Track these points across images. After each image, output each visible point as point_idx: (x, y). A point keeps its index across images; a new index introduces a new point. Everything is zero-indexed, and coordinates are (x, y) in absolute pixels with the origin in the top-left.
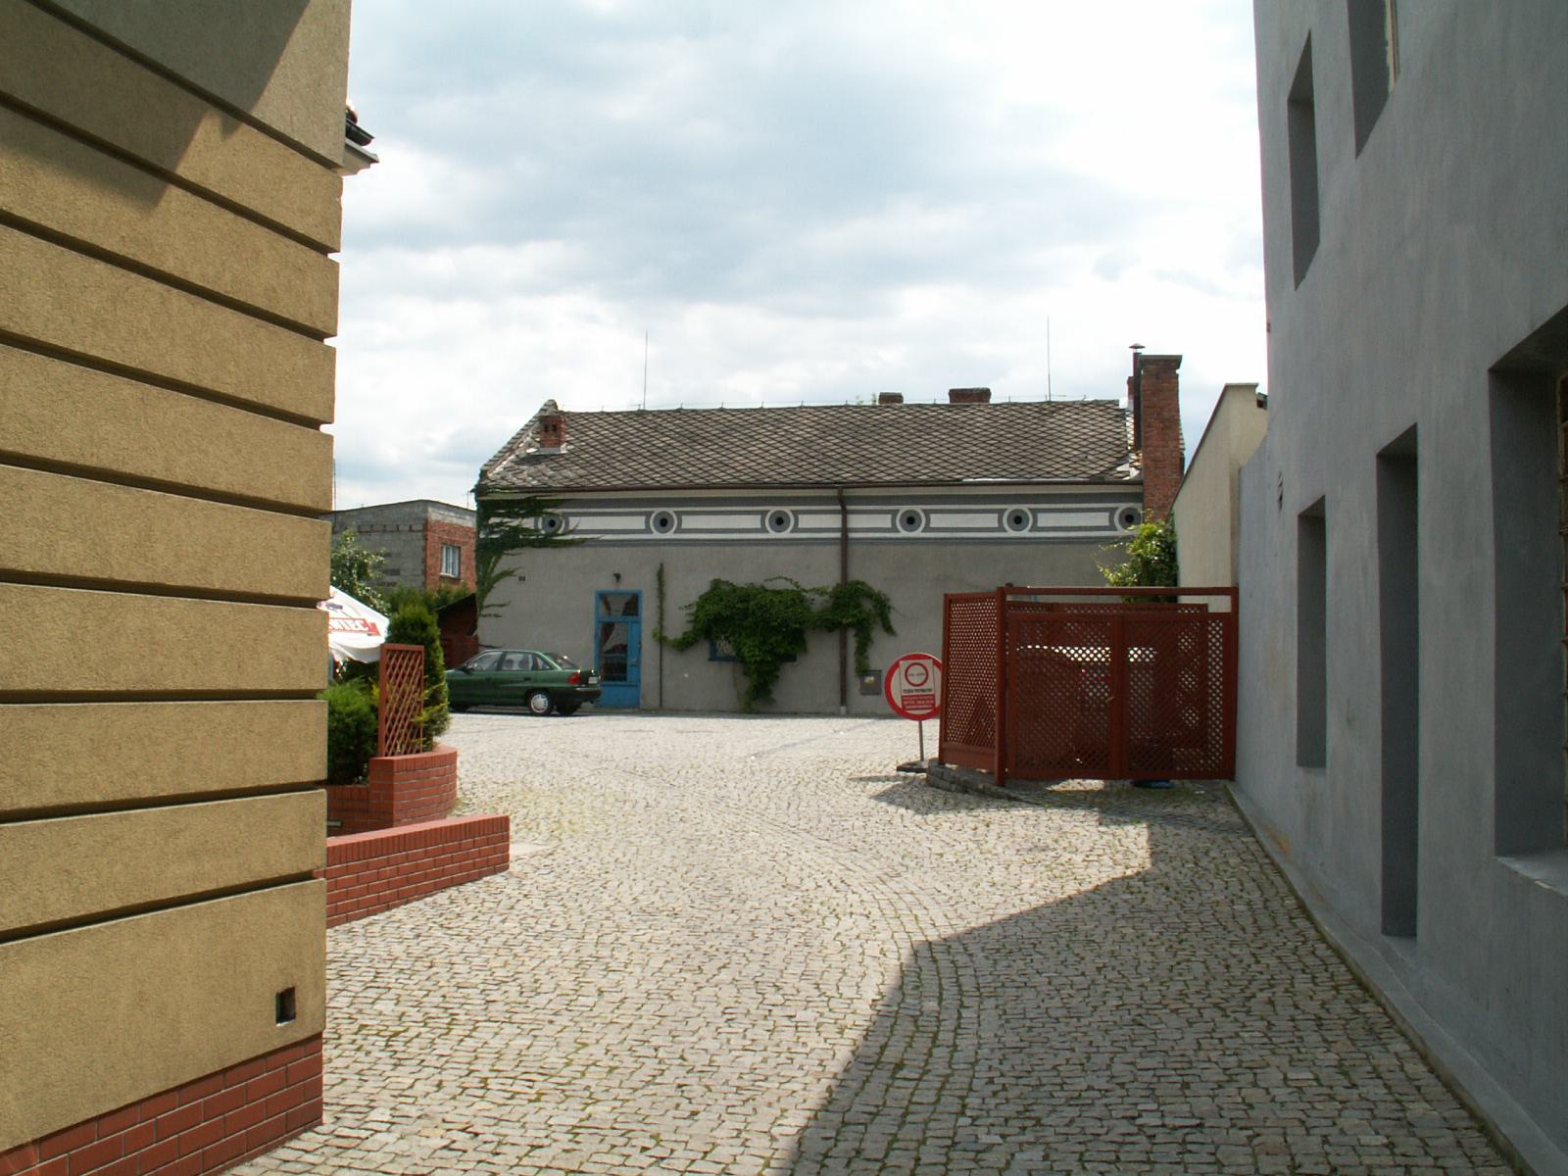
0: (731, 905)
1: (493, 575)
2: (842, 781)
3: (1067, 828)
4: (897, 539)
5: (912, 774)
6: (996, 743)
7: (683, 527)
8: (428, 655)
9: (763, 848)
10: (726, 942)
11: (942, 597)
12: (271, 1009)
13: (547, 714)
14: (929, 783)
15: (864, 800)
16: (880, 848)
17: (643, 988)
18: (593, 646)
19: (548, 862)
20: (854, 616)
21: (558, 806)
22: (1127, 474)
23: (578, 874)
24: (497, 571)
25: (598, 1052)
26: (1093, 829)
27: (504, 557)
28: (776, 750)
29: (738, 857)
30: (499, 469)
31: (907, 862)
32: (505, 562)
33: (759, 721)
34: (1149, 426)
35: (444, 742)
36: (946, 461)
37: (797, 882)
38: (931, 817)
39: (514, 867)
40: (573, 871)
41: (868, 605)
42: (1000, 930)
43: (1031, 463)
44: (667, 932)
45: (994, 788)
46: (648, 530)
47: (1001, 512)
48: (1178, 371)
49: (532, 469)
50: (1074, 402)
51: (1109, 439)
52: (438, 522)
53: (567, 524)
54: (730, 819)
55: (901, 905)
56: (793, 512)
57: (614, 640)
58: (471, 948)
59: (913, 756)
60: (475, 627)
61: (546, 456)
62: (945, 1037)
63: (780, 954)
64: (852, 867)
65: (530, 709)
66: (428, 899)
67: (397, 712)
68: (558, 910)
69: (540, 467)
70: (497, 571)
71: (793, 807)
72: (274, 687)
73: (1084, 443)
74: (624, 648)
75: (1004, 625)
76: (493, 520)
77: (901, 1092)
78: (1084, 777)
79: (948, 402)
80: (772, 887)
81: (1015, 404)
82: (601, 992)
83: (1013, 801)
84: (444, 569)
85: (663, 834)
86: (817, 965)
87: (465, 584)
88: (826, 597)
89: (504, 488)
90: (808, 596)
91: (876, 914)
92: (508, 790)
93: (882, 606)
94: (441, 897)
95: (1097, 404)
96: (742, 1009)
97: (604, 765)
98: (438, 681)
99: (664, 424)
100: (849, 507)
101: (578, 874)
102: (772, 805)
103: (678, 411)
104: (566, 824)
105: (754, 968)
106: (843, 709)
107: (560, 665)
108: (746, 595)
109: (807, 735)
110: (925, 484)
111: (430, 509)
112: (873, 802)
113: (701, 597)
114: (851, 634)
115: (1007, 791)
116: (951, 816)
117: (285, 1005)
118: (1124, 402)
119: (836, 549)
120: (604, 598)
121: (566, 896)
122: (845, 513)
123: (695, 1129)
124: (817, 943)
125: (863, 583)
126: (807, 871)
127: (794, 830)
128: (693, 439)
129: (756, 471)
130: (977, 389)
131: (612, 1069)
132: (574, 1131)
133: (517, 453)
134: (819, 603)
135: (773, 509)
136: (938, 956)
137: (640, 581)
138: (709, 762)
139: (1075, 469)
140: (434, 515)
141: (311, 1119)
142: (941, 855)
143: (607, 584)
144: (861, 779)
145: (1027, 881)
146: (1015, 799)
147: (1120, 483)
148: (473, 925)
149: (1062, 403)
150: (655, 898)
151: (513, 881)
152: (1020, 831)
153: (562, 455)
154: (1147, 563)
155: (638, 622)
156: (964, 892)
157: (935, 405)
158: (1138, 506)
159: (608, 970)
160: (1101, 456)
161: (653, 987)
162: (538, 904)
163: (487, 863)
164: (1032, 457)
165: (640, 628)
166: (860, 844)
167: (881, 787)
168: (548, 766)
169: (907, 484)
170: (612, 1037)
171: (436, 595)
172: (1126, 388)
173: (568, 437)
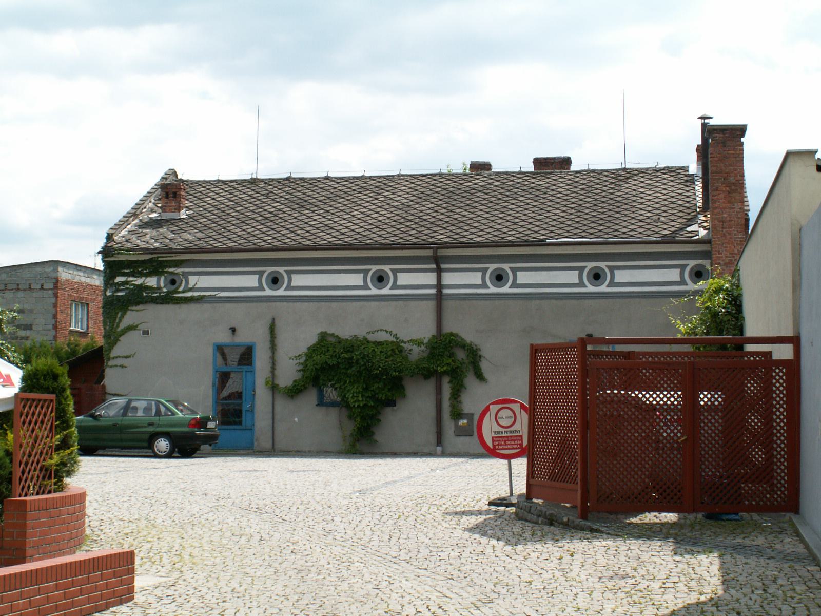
1: (119, 329)
2: (439, 515)
3: (645, 557)
5: (502, 509)
6: (579, 480)
8: (60, 403)
9: (367, 577)
11: (528, 348)
13: (169, 456)
15: (459, 532)
16: (474, 576)
19: (170, 592)
20: (449, 364)
21: (179, 540)
24: (123, 325)
27: (129, 313)
29: (345, 586)
31: (499, 588)
32: (130, 318)
34: (717, 190)
35: (74, 483)
38: (520, 548)
39: (139, 598)
40: (193, 600)
41: (461, 355)
45: (577, 521)
46: (260, 288)
47: (581, 270)
48: (743, 140)
49: (154, 233)
50: (647, 169)
51: (680, 202)
52: (67, 280)
53: (187, 282)
54: (338, 550)
57: (232, 386)
59: (503, 491)
60: (102, 377)
61: (167, 221)
64: (448, 594)
65: (154, 451)
67: (30, 456)
69: (161, 230)
70: (123, 325)
71: (394, 540)
73: (657, 206)
74: (239, 395)
75: (585, 372)
76: (119, 279)
78: (660, 510)
81: (594, 171)
83: (595, 532)
84: (73, 324)
85: (276, 565)
87: (92, 338)
88: (423, 348)
89: (128, 250)
95: (668, 170)
97: (222, 502)
98: (68, 426)
99: (275, 191)
100: (443, 266)
102: (375, 538)
103: (288, 179)
104: (187, 557)
106: (439, 449)
107: (181, 411)
108: (350, 346)
109: (406, 473)
110: (512, 244)
112: (467, 534)
113: (309, 349)
114: (446, 380)
116: (538, 546)
118: (694, 168)
119: (431, 305)
120: (220, 349)
122: (439, 271)
125: (456, 335)
126: (408, 597)
127: (395, 560)
130: (559, 158)
134: (416, 353)
135: (374, 268)
137: (254, 334)
138: (318, 498)
140: (64, 275)
142: (530, 583)
143: (224, 337)
144: (456, 513)
146: (597, 531)
149: (636, 170)
152: (602, 561)
153: (181, 220)
154: (715, 315)
155: (252, 372)
158: (706, 263)
160: (673, 217)
163: (114, 594)
166: (455, 573)
167: (474, 520)
168: (170, 504)
172: (694, 156)
173: (187, 203)
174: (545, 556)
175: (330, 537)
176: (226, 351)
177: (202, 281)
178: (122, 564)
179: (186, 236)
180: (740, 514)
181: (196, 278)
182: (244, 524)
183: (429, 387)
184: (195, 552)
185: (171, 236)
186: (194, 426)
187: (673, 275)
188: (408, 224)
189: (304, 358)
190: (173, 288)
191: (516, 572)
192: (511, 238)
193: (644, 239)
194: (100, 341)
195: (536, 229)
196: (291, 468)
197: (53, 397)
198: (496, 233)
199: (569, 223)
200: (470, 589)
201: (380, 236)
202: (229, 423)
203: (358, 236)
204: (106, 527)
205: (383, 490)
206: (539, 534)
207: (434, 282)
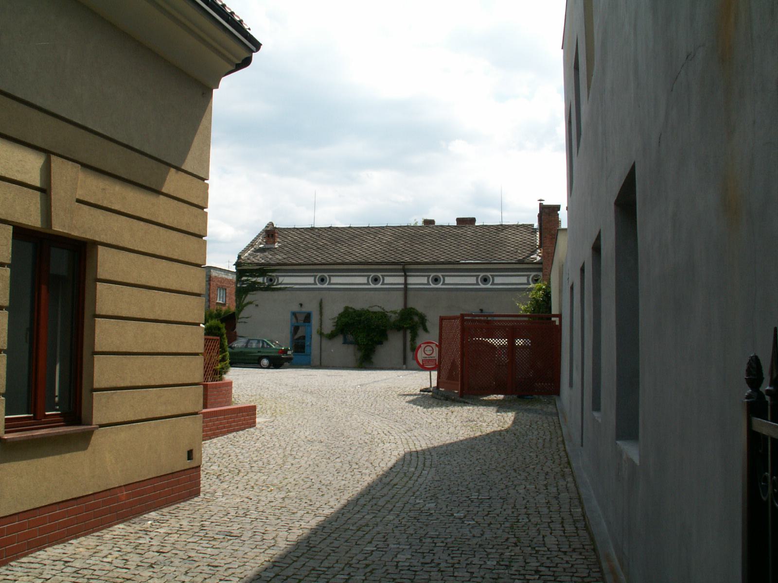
0: (343, 439)
1: (244, 303)
2: (396, 396)
3: (485, 413)
4: (429, 288)
5: (426, 393)
6: (460, 379)
7: (331, 282)
8: (221, 341)
9: (359, 421)
10: (340, 450)
11: (439, 318)
12: (186, 456)
13: (268, 368)
14: (433, 397)
15: (404, 403)
16: (407, 421)
17: (308, 463)
18: (289, 336)
19: (271, 424)
20: (410, 324)
21: (274, 404)
22: (535, 259)
23: (283, 428)
24: (245, 302)
25: (291, 480)
26: (495, 414)
27: (249, 295)
28: (369, 383)
29: (349, 423)
30: (246, 255)
31: (417, 426)
32: (249, 297)
33: (365, 372)
34: (545, 237)
35: (227, 377)
36: (452, 253)
37: (370, 432)
38: (430, 409)
39: (258, 426)
40: (281, 427)
41: (416, 319)
42: (446, 448)
43: (492, 254)
44: (317, 447)
45: (458, 398)
47: (477, 276)
48: (559, 212)
49: (262, 255)
50: (513, 225)
51: (528, 243)
52: (216, 277)
54: (347, 410)
55: (410, 440)
56: (382, 275)
57: (300, 333)
58: (244, 451)
59: (427, 385)
60: (235, 327)
61: (268, 249)
62: (414, 478)
63: (359, 454)
64: (394, 427)
65: (261, 365)
66: (225, 436)
67: (208, 364)
68: (276, 440)
69: (265, 254)
70: (245, 302)
71: (373, 406)
72: (188, 351)
73: (517, 244)
74: (304, 337)
75: (463, 330)
76: (244, 278)
77: (394, 491)
78: (498, 394)
79: (456, 224)
80: (360, 434)
81: (486, 226)
82: (292, 464)
83: (466, 403)
84: (218, 299)
85: (318, 415)
86: (372, 458)
87: (229, 307)
88: (397, 315)
89: (249, 264)
90: (389, 314)
91: (399, 442)
92: (253, 398)
93: (423, 319)
94: (231, 435)
95: (523, 226)
96: (343, 469)
97: (294, 389)
98: (225, 351)
99: (323, 234)
100: (408, 274)
101: (283, 428)
102: (364, 405)
103: (330, 227)
104: (278, 411)
105: (349, 458)
106: (404, 366)
107: (274, 345)
108: (360, 314)
109: (385, 377)
110: (443, 263)
111: (212, 271)
112: (407, 404)
113: (339, 315)
114: (408, 332)
115: (463, 400)
116: (438, 409)
117: (190, 455)
118: (536, 225)
119: (401, 293)
120: (294, 314)
121: (279, 436)
122: (406, 276)
123: (323, 498)
124: (374, 451)
125: (414, 309)
126: (375, 428)
127: (373, 414)
128: (336, 241)
129: (365, 256)
130: (469, 218)
131: (296, 484)
132: (283, 499)
133: (255, 247)
134: (394, 318)
135: (373, 274)
136: (419, 456)
137: (311, 307)
138: (340, 388)
139: (512, 257)
140: (214, 273)
141: (197, 494)
142: (431, 423)
143: (296, 308)
144: (404, 395)
145: (461, 432)
146: (467, 403)
147: (532, 263)
148: (244, 444)
149: (508, 225)
150: (314, 437)
151: (258, 431)
152: (465, 415)
153: (276, 248)
154: (537, 301)
155: (310, 326)
156: (436, 436)
157: (449, 226)
158: (540, 274)
159: (295, 458)
160: (524, 251)
161: (311, 463)
162: (268, 438)
163: (247, 424)
164: (492, 251)
165: (311, 329)
166: (399, 419)
167: (411, 398)
168: (270, 389)
169: (434, 263)
170: (296, 476)
171: (215, 312)
172: (537, 219)
173: (278, 240)
174: (440, 413)
175: (344, 405)
176: (297, 315)
177: (286, 280)
178: (250, 411)
179: (278, 257)
180: (534, 396)
181: (283, 278)
182: (304, 398)
183: (400, 335)
184: (282, 409)
185: (270, 257)
186: (281, 353)
187: (524, 280)
188: (391, 252)
189: (336, 320)
190: (270, 283)
191: (426, 419)
192: (442, 260)
193: (509, 262)
194: (233, 308)
195: (455, 255)
196: (329, 374)
197: (219, 338)
198: (435, 257)
199: (472, 252)
200: (404, 426)
201: (376, 258)
202: (299, 352)
203: (364, 258)
204: (241, 397)
205: (372, 385)
206: (440, 404)
207: (403, 282)
